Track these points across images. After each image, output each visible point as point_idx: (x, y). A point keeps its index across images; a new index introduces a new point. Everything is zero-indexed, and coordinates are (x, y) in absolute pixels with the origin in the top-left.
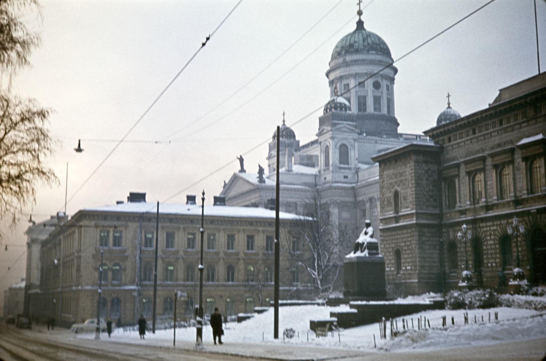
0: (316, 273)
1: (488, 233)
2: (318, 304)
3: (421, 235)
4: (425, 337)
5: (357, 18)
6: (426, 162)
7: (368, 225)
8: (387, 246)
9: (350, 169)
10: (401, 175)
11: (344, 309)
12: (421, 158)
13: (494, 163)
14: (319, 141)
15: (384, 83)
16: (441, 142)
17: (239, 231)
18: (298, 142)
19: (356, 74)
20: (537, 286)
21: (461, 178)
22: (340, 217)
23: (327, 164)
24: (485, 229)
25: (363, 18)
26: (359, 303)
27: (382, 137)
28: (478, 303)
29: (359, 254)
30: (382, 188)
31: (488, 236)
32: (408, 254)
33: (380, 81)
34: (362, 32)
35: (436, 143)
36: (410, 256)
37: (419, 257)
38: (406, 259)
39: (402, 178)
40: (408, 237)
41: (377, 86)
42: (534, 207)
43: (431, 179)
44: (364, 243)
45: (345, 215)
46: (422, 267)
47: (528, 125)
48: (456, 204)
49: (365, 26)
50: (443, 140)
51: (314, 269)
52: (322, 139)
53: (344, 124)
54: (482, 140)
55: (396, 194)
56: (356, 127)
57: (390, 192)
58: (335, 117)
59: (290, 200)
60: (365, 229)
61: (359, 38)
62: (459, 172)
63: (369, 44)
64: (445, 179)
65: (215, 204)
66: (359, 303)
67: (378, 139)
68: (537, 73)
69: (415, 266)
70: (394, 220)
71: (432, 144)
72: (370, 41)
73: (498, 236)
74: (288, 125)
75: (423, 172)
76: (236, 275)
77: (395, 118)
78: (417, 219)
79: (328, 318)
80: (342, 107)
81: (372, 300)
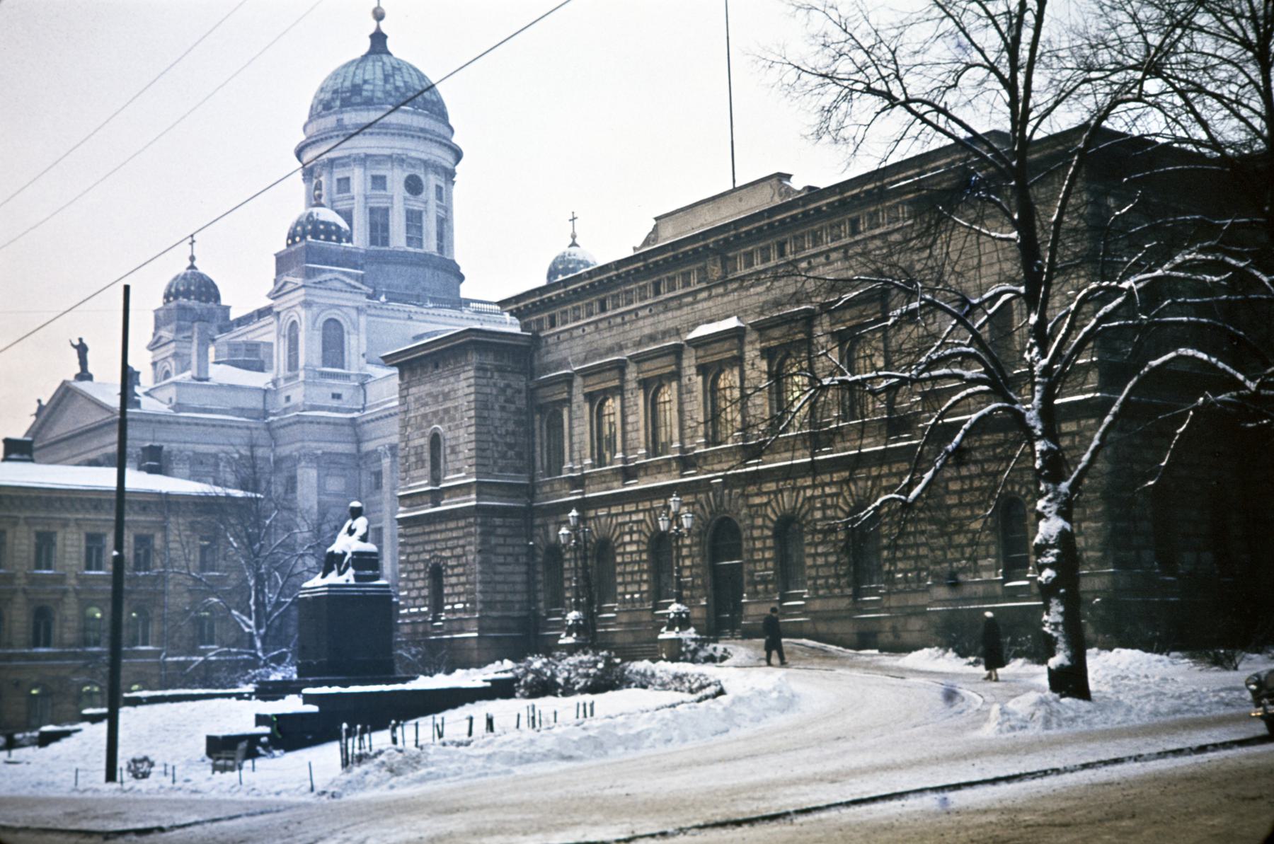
0: (252, 623)
1: (627, 529)
2: (240, 696)
3: (486, 534)
4: (418, 762)
5: (371, 27)
6: (501, 370)
7: (356, 513)
8: (413, 558)
9: (347, 377)
10: (446, 396)
11: (292, 704)
12: (490, 360)
13: (641, 376)
14: (275, 310)
15: (431, 181)
16: (534, 327)
17: (65, 524)
18: (227, 308)
19: (367, 156)
20: (716, 641)
21: (574, 407)
22: (321, 489)
23: (293, 364)
24: (620, 519)
25: (385, 27)
26: (325, 690)
27: (421, 306)
28: (582, 682)
29: (333, 578)
30: (405, 425)
31: (818, 509)
32: (458, 575)
33: (422, 177)
34: (381, 60)
35: (525, 327)
36: (463, 579)
37: (481, 582)
38: (452, 585)
39: (449, 404)
40: (458, 538)
41: (414, 186)
42: (714, 474)
43: (513, 407)
44: (345, 554)
45: (335, 484)
46: (488, 605)
47: (710, 297)
48: (564, 464)
49: (390, 45)
50: (540, 321)
51: (246, 611)
52: (280, 305)
53: (333, 272)
54: (619, 325)
55: (435, 440)
56: (361, 279)
57: (423, 435)
58: (313, 254)
59: (201, 448)
60: (349, 522)
61: (373, 72)
62: (570, 393)
63: (397, 88)
64: (541, 409)
65: (6, 459)
66: (325, 690)
67: (414, 308)
68: (731, 187)
69: (473, 602)
70: (427, 498)
71: (517, 330)
72: (400, 84)
73: (771, 520)
74: (202, 268)
75: (495, 392)
76: (56, 631)
77: (453, 261)
78: (477, 500)
79: (250, 728)
80: (329, 231)
81: (354, 684)
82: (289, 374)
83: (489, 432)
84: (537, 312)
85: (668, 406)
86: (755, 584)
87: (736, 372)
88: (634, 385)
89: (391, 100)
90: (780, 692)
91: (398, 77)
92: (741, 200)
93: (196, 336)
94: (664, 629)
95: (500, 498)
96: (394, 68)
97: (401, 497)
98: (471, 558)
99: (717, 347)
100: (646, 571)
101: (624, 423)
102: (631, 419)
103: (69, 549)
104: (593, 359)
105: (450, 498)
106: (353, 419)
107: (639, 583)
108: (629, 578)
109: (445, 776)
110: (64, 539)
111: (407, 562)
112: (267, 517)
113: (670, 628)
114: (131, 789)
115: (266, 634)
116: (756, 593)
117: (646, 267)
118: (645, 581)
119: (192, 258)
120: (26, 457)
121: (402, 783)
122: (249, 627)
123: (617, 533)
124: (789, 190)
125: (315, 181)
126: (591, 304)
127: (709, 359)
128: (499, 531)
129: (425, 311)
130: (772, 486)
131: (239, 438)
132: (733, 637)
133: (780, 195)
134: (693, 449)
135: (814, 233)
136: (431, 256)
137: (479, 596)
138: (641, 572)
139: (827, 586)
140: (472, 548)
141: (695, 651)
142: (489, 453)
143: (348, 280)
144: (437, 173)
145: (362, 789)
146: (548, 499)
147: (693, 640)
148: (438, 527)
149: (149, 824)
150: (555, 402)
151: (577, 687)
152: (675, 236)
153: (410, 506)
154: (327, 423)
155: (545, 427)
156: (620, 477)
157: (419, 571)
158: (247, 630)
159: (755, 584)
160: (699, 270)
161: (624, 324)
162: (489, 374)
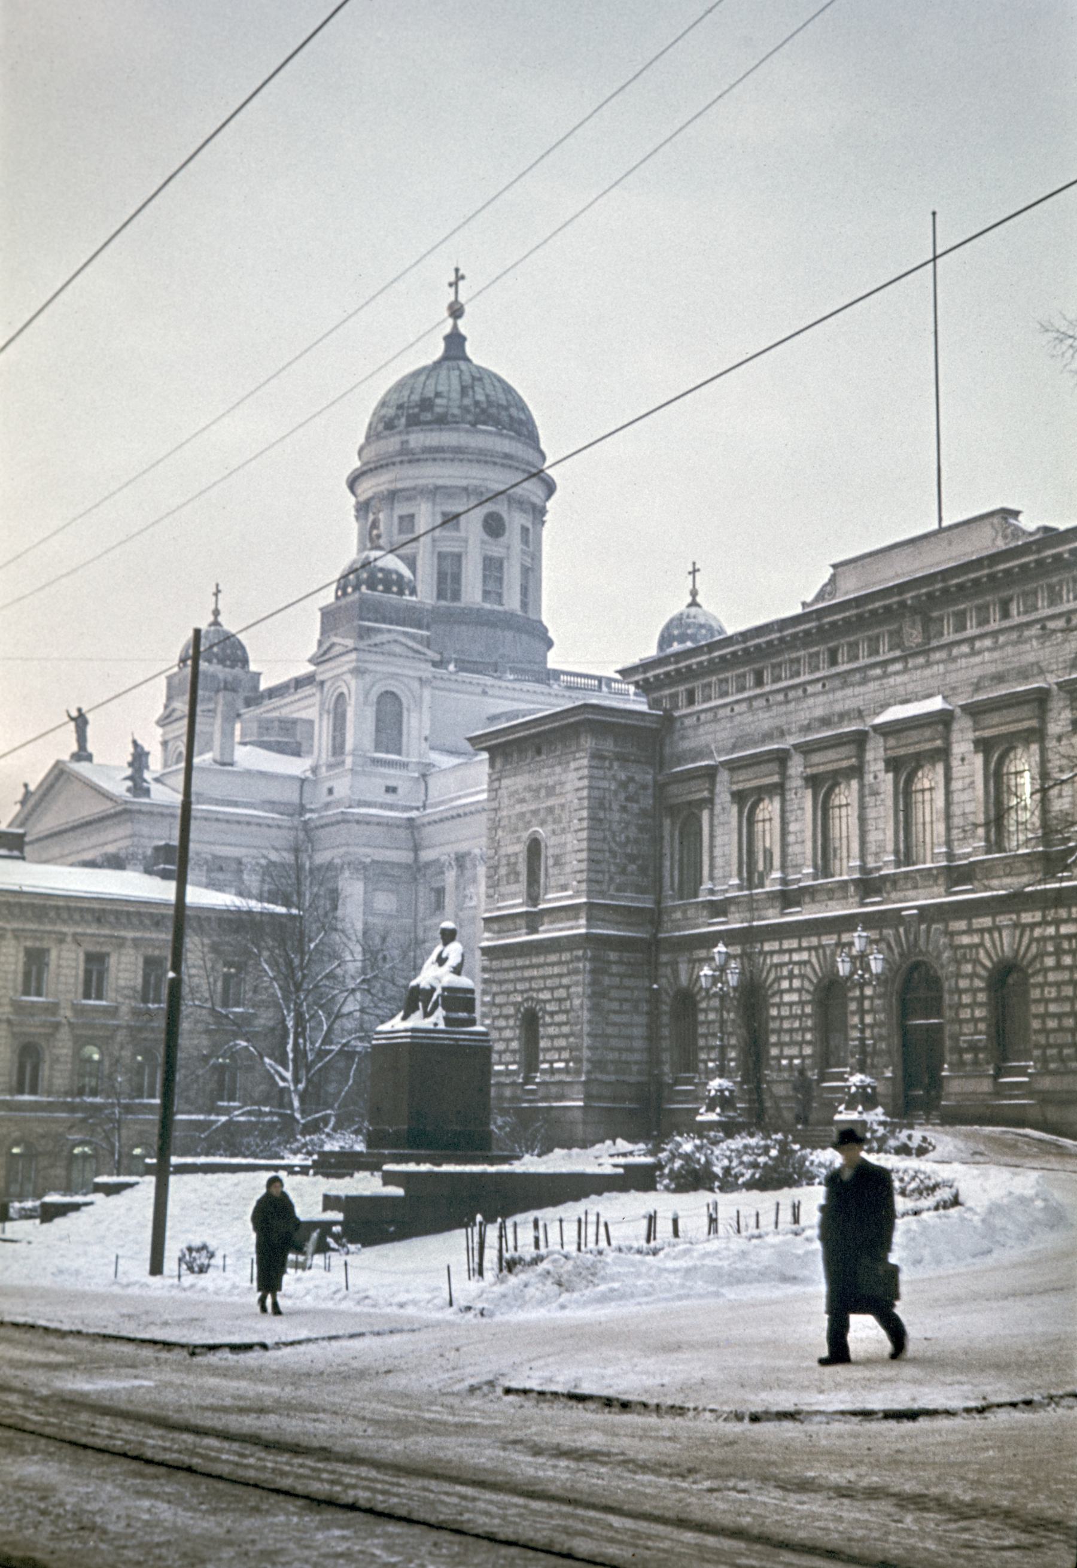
0: (288, 1075)
1: (785, 972)
6: (623, 759)
7: (448, 936)
8: (499, 1000)
9: (405, 765)
10: (551, 791)
12: (609, 746)
13: (809, 771)
14: (319, 678)
15: (516, 520)
17: (61, 939)
19: (437, 488)
20: (911, 1126)
21: (718, 809)
22: (367, 904)
23: (338, 749)
24: (776, 959)
26: (412, 1167)
27: (499, 678)
28: (748, 1174)
29: (417, 1020)
30: (494, 826)
31: (1050, 954)
32: (560, 1025)
33: (505, 516)
35: (654, 704)
36: (566, 1029)
38: (552, 1038)
39: (551, 802)
40: (560, 976)
41: (494, 526)
43: (635, 807)
44: (433, 989)
45: (385, 902)
46: (598, 1065)
47: (906, 670)
48: (701, 884)
49: (469, 349)
50: (674, 697)
52: (325, 673)
53: (390, 632)
54: (780, 704)
55: (534, 848)
56: (428, 643)
58: (369, 610)
60: (439, 948)
61: (449, 383)
62: (712, 791)
63: (477, 403)
64: (672, 811)
66: (412, 1167)
67: (489, 681)
68: (935, 526)
69: (578, 1060)
70: (521, 922)
71: (644, 708)
72: (481, 397)
73: (984, 967)
76: (45, 1071)
78: (588, 926)
80: (392, 582)
81: (449, 1160)
82: (332, 760)
83: (604, 839)
84: (671, 685)
85: (844, 811)
86: (961, 1051)
87: (940, 768)
88: (799, 782)
89: (470, 418)
90: (1045, 1200)
91: (478, 389)
92: (950, 544)
93: (220, 709)
94: (842, 1108)
95: (616, 924)
96: (473, 378)
97: (486, 920)
98: (577, 1002)
99: (914, 735)
100: (809, 1029)
101: (784, 833)
102: (793, 827)
103: (65, 971)
104: (743, 747)
105: (552, 922)
106: (411, 820)
107: (801, 1044)
108: (786, 1038)
109: (632, 1295)
110: (59, 957)
111: (493, 1004)
112: (310, 941)
113: (850, 1106)
114: (192, 1286)
115: (306, 1090)
116: (962, 1063)
117: (820, 628)
118: (809, 1043)
119: (216, 613)
120: (16, 853)
121: (576, 1302)
122: (284, 1079)
123: (772, 976)
124: (1018, 532)
125: (371, 517)
126: (744, 675)
127: (902, 752)
128: (614, 969)
129: (504, 684)
130: (986, 922)
131: (283, 837)
132: (928, 1122)
133: (1005, 537)
134: (879, 869)
135: (1051, 588)
136: (513, 614)
137: (586, 1053)
138: (803, 1030)
139: (1062, 1059)
140: (580, 989)
141: (882, 1140)
142: (604, 866)
143: (411, 643)
144: (524, 511)
145: (521, 1307)
146: (679, 929)
147: (881, 1123)
148: (535, 960)
149: (247, 1339)
150: (690, 803)
151: (741, 1181)
152: (862, 588)
153: (499, 932)
154: (379, 824)
155: (677, 833)
156: (777, 904)
157: (507, 1017)
158: (282, 1084)
159: (961, 1051)
160: (891, 634)
161: (787, 702)
162: (607, 764)
